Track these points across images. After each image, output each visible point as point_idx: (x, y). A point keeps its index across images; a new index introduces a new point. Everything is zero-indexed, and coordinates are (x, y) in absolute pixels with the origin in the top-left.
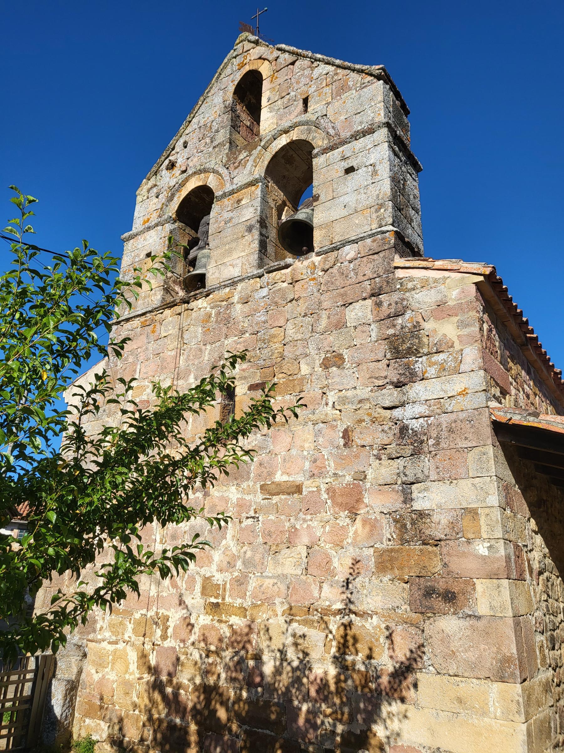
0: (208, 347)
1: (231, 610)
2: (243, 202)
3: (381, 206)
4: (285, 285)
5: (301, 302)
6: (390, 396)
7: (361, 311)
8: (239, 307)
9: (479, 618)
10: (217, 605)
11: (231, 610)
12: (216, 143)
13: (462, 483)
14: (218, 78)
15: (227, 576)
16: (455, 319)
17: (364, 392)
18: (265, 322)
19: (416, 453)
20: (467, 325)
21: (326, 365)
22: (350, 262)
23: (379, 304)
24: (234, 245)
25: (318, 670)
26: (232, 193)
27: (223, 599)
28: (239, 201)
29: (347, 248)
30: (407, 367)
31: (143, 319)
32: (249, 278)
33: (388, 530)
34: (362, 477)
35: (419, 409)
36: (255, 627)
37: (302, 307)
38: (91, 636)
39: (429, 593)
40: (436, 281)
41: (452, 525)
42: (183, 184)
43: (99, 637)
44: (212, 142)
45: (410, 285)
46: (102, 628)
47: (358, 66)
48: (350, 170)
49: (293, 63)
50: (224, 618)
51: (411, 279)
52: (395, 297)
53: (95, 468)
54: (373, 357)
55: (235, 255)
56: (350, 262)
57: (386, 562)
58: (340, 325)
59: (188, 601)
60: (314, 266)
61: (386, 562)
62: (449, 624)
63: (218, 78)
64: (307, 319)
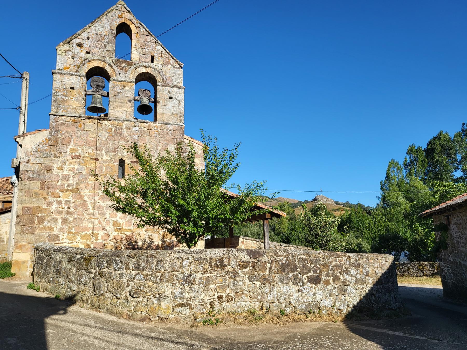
0: (112, 142)
1: (126, 230)
2: (126, 88)
3: (181, 116)
4: (145, 129)
5: (152, 137)
8: (125, 130)
10: (120, 229)
11: (126, 230)
12: (107, 49)
14: (107, 14)
15: (124, 221)
22: (170, 130)
24: (123, 104)
25: (156, 243)
27: (122, 227)
28: (124, 86)
29: (169, 125)
31: (73, 119)
32: (130, 121)
36: (134, 234)
37: (153, 139)
38: (57, 242)
42: (437, 204)
43: (61, 242)
47: (175, 58)
48: (171, 98)
49: (147, 36)
50: (123, 232)
55: (123, 109)
56: (170, 130)
59: (107, 228)
60: (157, 127)
63: (107, 14)
64: (154, 144)
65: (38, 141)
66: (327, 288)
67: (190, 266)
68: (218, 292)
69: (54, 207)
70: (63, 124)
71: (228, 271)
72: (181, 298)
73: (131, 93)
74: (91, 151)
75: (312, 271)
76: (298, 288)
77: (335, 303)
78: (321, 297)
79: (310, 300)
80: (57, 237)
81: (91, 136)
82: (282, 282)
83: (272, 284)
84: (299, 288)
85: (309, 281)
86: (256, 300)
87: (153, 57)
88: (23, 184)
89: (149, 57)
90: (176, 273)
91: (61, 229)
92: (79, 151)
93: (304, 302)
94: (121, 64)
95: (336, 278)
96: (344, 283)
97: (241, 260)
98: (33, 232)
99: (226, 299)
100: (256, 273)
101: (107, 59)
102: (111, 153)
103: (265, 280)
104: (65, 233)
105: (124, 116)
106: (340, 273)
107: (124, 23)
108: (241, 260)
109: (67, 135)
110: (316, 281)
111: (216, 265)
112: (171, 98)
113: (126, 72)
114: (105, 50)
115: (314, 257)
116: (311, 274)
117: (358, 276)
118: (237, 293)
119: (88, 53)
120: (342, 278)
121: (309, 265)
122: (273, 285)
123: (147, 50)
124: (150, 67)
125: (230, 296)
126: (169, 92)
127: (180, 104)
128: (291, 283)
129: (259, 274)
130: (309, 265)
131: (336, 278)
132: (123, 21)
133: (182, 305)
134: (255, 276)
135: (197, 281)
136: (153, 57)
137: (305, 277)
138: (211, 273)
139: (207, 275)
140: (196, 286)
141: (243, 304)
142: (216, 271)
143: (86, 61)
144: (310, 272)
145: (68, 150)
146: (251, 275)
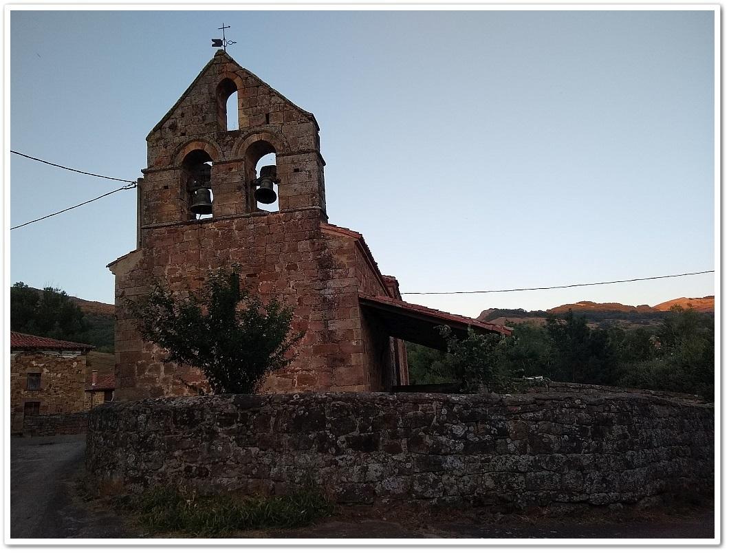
0: (219, 251)
2: (233, 170)
3: (314, 195)
4: (264, 225)
6: (319, 285)
7: (304, 245)
9: (352, 366)
12: (207, 122)
13: (347, 320)
16: (346, 255)
17: (307, 282)
18: (253, 243)
19: (330, 308)
20: (351, 259)
21: (288, 268)
23: (314, 244)
26: (226, 162)
29: (297, 213)
30: (326, 273)
31: (168, 228)
33: (318, 338)
34: (307, 317)
35: (331, 291)
39: (335, 360)
40: (339, 237)
41: (343, 335)
44: (204, 120)
45: (327, 237)
46: (167, 393)
48: (296, 170)
51: (328, 234)
52: (321, 241)
53: (614, 463)
54: (310, 267)
57: (317, 351)
58: (295, 250)
61: (317, 351)
62: (342, 370)
65: (131, 267)
66: (393, 459)
67: (146, 423)
68: (185, 462)
69: (155, 351)
70: (158, 238)
71: (201, 430)
72: (134, 469)
73: (239, 177)
74: (193, 268)
75: (357, 429)
76: (328, 457)
77: (412, 485)
78: (379, 474)
79: (355, 479)
80: (160, 392)
81: (193, 248)
82: (297, 448)
83: (277, 449)
84: (330, 457)
85: (349, 446)
86: (249, 476)
87: (267, 116)
88: (119, 323)
89: (262, 117)
90: (131, 433)
91: (165, 379)
92: (180, 271)
93: (342, 482)
94: (224, 139)
95: (415, 442)
96: (436, 450)
97: (221, 412)
98: (133, 386)
99: (197, 472)
100: (249, 433)
101: (206, 137)
102: (219, 268)
103: (265, 445)
104: (169, 384)
105: (233, 212)
106: (425, 432)
107: (227, 78)
108: (221, 412)
109: (163, 252)
110: (366, 445)
111: (183, 422)
112: (296, 170)
113: (232, 147)
114: (203, 125)
115: (362, 403)
116: (356, 433)
117: (471, 437)
118: (215, 463)
119: (183, 134)
120: (428, 440)
121: (352, 417)
122: (280, 452)
123: (259, 108)
124: (262, 131)
125: (205, 468)
126: (293, 162)
127: (310, 176)
128: (315, 447)
129: (255, 434)
130: (352, 417)
131: (415, 442)
132: (225, 76)
133: (135, 480)
134: (249, 436)
135: (156, 444)
136: (267, 116)
137: (342, 438)
138: (175, 433)
139: (170, 436)
140: (156, 453)
141: (225, 481)
142: (183, 429)
143: (183, 146)
144: (353, 429)
145: (166, 272)
146: (241, 436)
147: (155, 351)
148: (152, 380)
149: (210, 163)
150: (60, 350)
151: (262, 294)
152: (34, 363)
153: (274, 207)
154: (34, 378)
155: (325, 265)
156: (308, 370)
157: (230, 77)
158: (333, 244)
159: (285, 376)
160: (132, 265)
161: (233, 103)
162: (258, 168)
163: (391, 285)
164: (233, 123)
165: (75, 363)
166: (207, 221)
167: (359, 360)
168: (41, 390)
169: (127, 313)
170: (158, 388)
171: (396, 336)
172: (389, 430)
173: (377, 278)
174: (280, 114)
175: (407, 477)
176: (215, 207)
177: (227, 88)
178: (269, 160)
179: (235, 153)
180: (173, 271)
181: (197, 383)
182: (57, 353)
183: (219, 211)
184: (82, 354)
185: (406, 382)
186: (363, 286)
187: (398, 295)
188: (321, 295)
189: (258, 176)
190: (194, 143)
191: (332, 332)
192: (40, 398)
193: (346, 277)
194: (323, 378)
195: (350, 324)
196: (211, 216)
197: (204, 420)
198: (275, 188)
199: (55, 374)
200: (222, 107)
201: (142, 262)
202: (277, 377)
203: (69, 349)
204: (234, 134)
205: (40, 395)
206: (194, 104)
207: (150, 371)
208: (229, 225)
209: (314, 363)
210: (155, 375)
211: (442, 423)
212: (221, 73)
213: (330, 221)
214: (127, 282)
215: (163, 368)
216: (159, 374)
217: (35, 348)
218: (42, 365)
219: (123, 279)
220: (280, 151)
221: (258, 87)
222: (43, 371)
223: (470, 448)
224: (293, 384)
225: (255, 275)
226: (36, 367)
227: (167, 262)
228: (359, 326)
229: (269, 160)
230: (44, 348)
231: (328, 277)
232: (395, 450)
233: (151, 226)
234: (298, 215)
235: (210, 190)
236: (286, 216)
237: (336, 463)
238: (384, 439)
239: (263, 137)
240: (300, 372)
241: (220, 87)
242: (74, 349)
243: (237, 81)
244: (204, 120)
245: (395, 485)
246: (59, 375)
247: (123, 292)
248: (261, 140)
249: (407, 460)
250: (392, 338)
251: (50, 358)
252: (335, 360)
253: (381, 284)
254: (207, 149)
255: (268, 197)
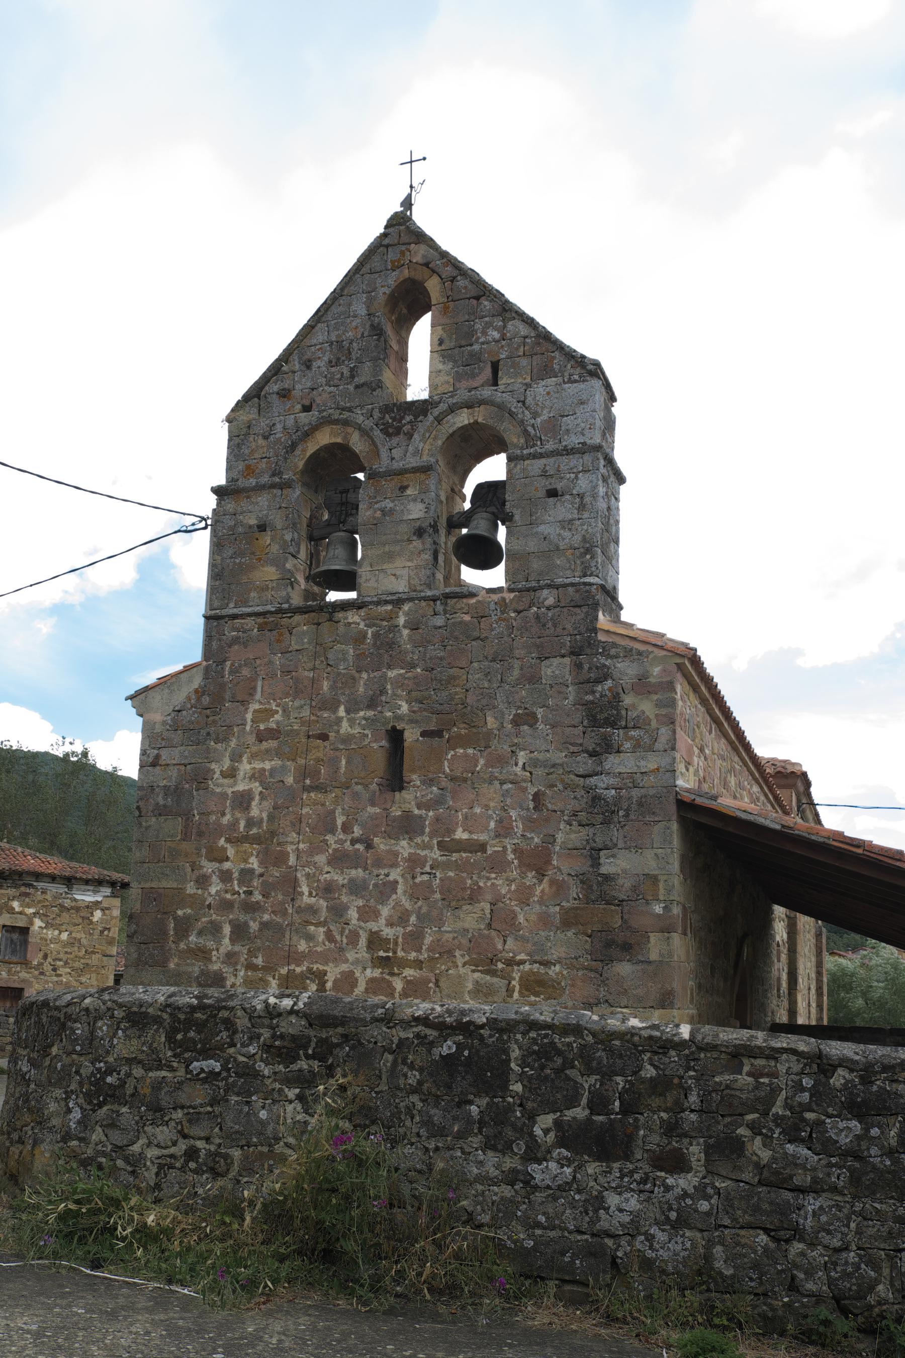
6: (585, 763)
7: (557, 668)
19: (606, 822)
21: (517, 722)
29: (545, 592)
31: (260, 620)
34: (551, 839)
40: (640, 653)
41: (634, 888)
45: (613, 652)
48: (553, 493)
51: (614, 645)
54: (567, 721)
57: (569, 920)
58: (533, 679)
61: (569, 920)
62: (624, 969)
69: (213, 890)
70: (235, 641)
73: (421, 506)
85: (561, 1142)
92: (277, 717)
95: (726, 1149)
104: (239, 967)
106: (755, 1129)
109: (246, 672)
110: (601, 1142)
116: (579, 1112)
119: (307, 409)
120: (759, 1150)
131: (726, 1149)
132: (406, 273)
137: (546, 1120)
144: (572, 1102)
145: (249, 716)
147: (213, 890)
148: (203, 954)
149: (361, 476)
150: (69, 881)
151: (453, 779)
152: (16, 905)
153: (494, 578)
154: (15, 936)
155: (604, 720)
156: (546, 964)
157: (418, 277)
158: (626, 670)
159: (493, 973)
160: (180, 697)
161: (421, 336)
162: (469, 489)
163: (790, 782)
164: (418, 385)
165: (98, 914)
166: (344, 606)
167: (675, 951)
168: (25, 963)
169: (162, 802)
170: (215, 972)
171: (796, 905)
172: (664, 1115)
173: (742, 759)
174: (524, 362)
175: (699, 1235)
176: (364, 574)
177: (409, 303)
178: (493, 469)
179: (424, 446)
180: (265, 714)
181: (298, 970)
182: (62, 889)
183: (372, 584)
184: (113, 895)
185: (820, 1018)
186: (696, 772)
187: (807, 804)
188: (588, 789)
189: (467, 505)
190: (327, 430)
191: (607, 878)
192: (23, 981)
193: (651, 749)
194: (579, 983)
195: (655, 861)
196: (353, 595)
197: (235, 1045)
198: (502, 534)
199: (56, 932)
200: (395, 347)
201: (199, 693)
202: (473, 971)
203: (87, 882)
204: (420, 408)
205: (23, 975)
206: (334, 339)
207: (200, 933)
208: (390, 617)
209: (562, 945)
210: (211, 944)
211: (798, 1111)
212: (397, 266)
213: (625, 616)
214: (165, 734)
215: (227, 930)
216: (219, 943)
217: (20, 874)
218: (32, 911)
219: (158, 728)
220: (516, 446)
221: (477, 298)
222: (32, 923)
223: (863, 1182)
224: (510, 991)
225: (438, 734)
226: (20, 913)
227: (252, 695)
228: (676, 866)
229: (493, 469)
230: (38, 876)
231: (607, 747)
232: (677, 1163)
233: (225, 612)
234: (549, 598)
235: (357, 536)
236: (518, 599)
237: (528, 1180)
238: (649, 1137)
239: (480, 415)
240: (527, 967)
241: (393, 300)
242: (99, 883)
243: (433, 286)
244: (352, 377)
245: (670, 1248)
246: (64, 936)
247: (158, 757)
248: (476, 422)
249: (701, 1191)
250: (779, 911)
251: (49, 897)
252: (609, 944)
253: (752, 774)
254: (357, 444)
255: (483, 554)
